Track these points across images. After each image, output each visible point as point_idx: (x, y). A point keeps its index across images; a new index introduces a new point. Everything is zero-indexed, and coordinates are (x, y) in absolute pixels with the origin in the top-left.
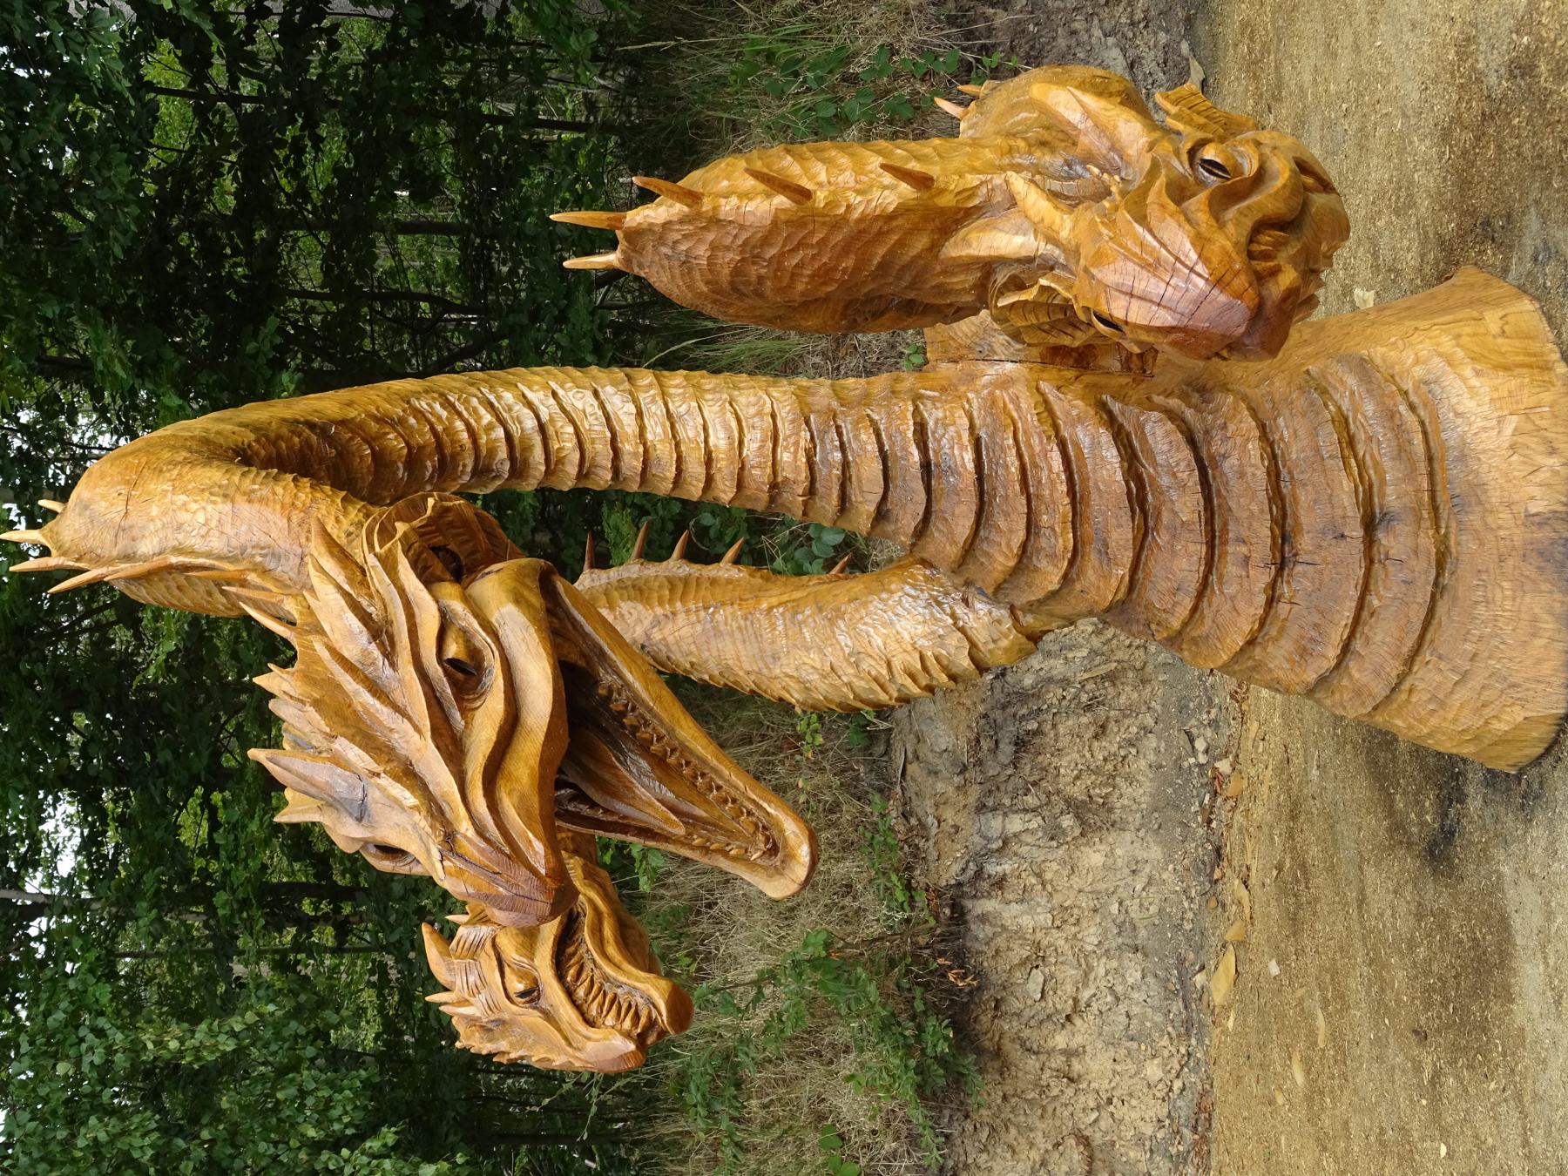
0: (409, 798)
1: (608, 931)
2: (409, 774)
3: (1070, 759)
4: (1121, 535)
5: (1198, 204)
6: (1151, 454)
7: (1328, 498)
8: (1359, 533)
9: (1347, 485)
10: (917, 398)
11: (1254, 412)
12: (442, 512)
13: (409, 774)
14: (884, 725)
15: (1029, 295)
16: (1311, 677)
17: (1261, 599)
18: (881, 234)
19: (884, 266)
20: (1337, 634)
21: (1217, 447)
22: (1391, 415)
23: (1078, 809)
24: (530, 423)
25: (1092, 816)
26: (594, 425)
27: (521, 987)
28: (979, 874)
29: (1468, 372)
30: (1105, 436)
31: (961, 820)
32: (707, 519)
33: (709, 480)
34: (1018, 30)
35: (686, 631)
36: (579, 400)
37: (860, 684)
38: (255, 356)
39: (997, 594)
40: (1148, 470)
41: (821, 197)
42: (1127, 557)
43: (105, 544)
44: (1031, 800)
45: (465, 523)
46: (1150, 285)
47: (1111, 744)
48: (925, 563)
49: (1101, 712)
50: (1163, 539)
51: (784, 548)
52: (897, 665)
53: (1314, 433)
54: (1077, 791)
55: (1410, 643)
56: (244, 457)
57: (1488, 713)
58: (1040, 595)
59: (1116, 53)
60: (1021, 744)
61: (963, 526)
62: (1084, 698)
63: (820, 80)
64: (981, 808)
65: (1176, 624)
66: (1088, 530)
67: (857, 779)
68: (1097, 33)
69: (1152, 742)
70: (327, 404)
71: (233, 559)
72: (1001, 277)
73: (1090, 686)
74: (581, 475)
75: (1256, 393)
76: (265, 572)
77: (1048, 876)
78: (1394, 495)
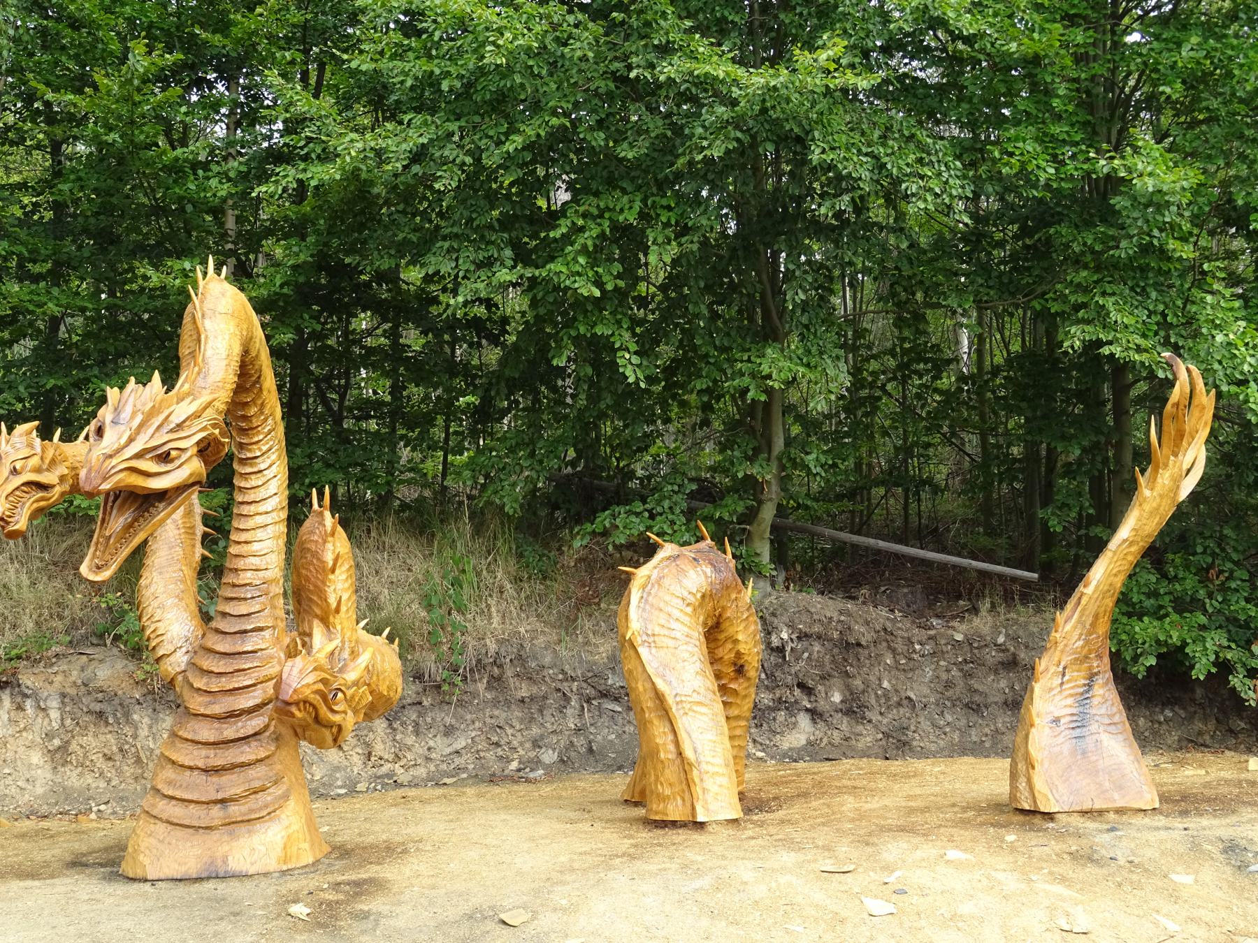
0: (123, 441)
1: (42, 503)
2: (131, 440)
3: (93, 742)
4: (217, 709)
5: (321, 686)
6: (250, 719)
7: (232, 785)
8: (219, 798)
9: (238, 792)
10: (274, 627)
11: (267, 757)
12: (223, 444)
13: (131, 440)
14: (108, 642)
15: (300, 647)
16: (159, 787)
17: (192, 764)
18: (320, 598)
19: (311, 600)
20: (178, 794)
21: (254, 744)
22: (266, 806)
23: (64, 748)
24: (262, 467)
25: (59, 755)
26: (262, 493)
27: (18, 467)
28: (26, 696)
29: (283, 833)
30: (258, 701)
31: (56, 685)
32: (222, 544)
33: (239, 543)
34: (475, 695)
35: (171, 534)
36: (273, 487)
37: (150, 609)
38: (302, 317)
39: (192, 664)
40: (244, 718)
41: (332, 577)
42: (208, 712)
43: (208, 305)
44: (68, 722)
45: (219, 453)
46: (295, 671)
47: (100, 763)
48: (204, 635)
49: (118, 757)
50: (216, 725)
51: (207, 585)
52: (158, 624)
53: (259, 779)
54: (74, 746)
55: (176, 821)
56: (246, 352)
57: (147, 852)
58: (191, 680)
59: (464, 744)
60: (100, 714)
61: (220, 647)
62: (126, 747)
63: (450, 597)
64: (63, 695)
65: (180, 733)
66: (219, 696)
67: (77, 629)
68: (473, 734)
69: (103, 784)
70: (269, 382)
71: (203, 360)
72: (306, 639)
73: (133, 750)
74: (240, 488)
75: (275, 758)
76: (198, 374)
77: (24, 734)
78: (235, 810)
